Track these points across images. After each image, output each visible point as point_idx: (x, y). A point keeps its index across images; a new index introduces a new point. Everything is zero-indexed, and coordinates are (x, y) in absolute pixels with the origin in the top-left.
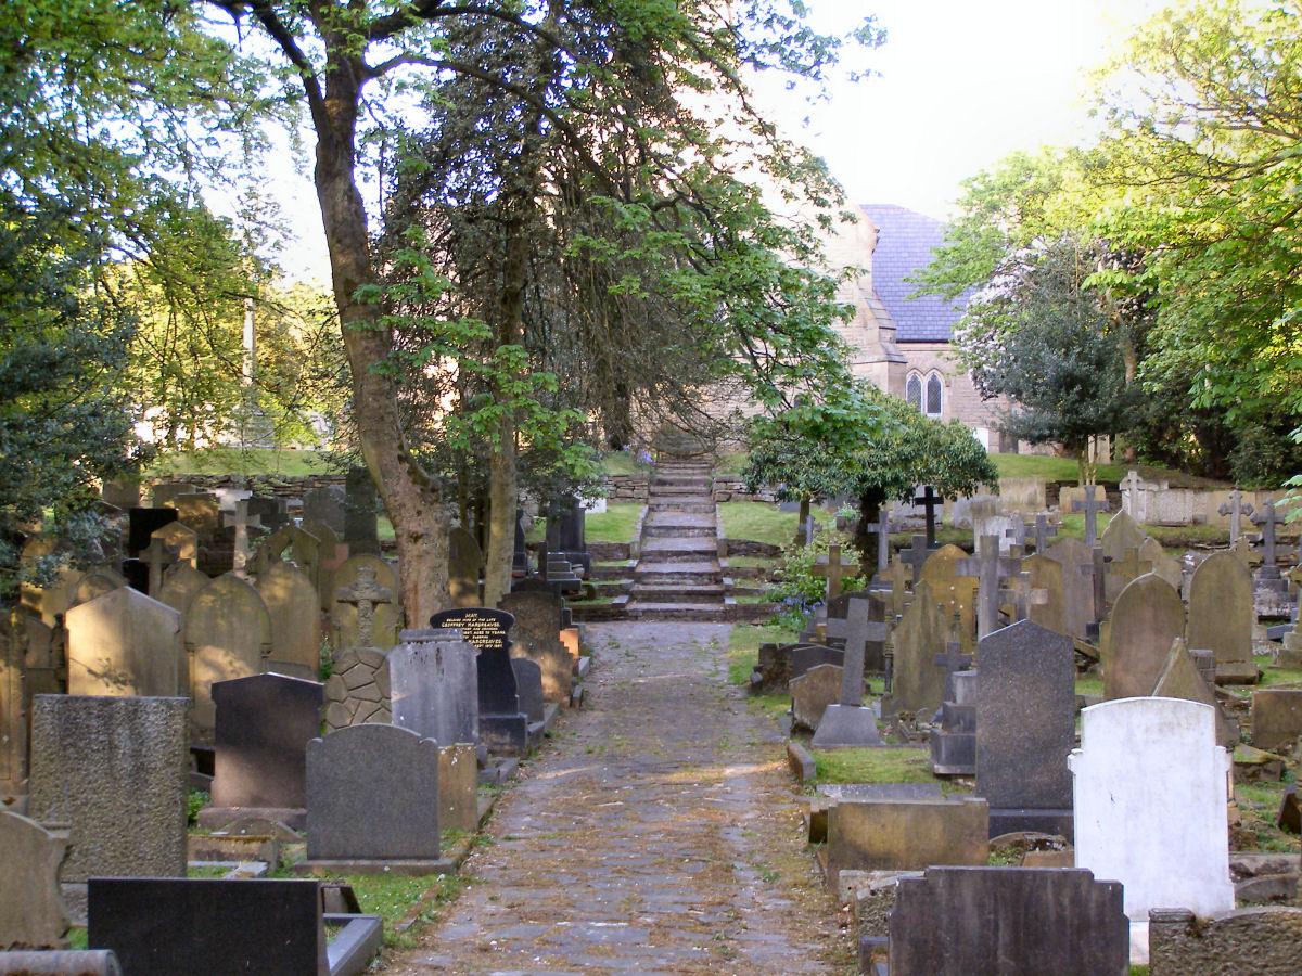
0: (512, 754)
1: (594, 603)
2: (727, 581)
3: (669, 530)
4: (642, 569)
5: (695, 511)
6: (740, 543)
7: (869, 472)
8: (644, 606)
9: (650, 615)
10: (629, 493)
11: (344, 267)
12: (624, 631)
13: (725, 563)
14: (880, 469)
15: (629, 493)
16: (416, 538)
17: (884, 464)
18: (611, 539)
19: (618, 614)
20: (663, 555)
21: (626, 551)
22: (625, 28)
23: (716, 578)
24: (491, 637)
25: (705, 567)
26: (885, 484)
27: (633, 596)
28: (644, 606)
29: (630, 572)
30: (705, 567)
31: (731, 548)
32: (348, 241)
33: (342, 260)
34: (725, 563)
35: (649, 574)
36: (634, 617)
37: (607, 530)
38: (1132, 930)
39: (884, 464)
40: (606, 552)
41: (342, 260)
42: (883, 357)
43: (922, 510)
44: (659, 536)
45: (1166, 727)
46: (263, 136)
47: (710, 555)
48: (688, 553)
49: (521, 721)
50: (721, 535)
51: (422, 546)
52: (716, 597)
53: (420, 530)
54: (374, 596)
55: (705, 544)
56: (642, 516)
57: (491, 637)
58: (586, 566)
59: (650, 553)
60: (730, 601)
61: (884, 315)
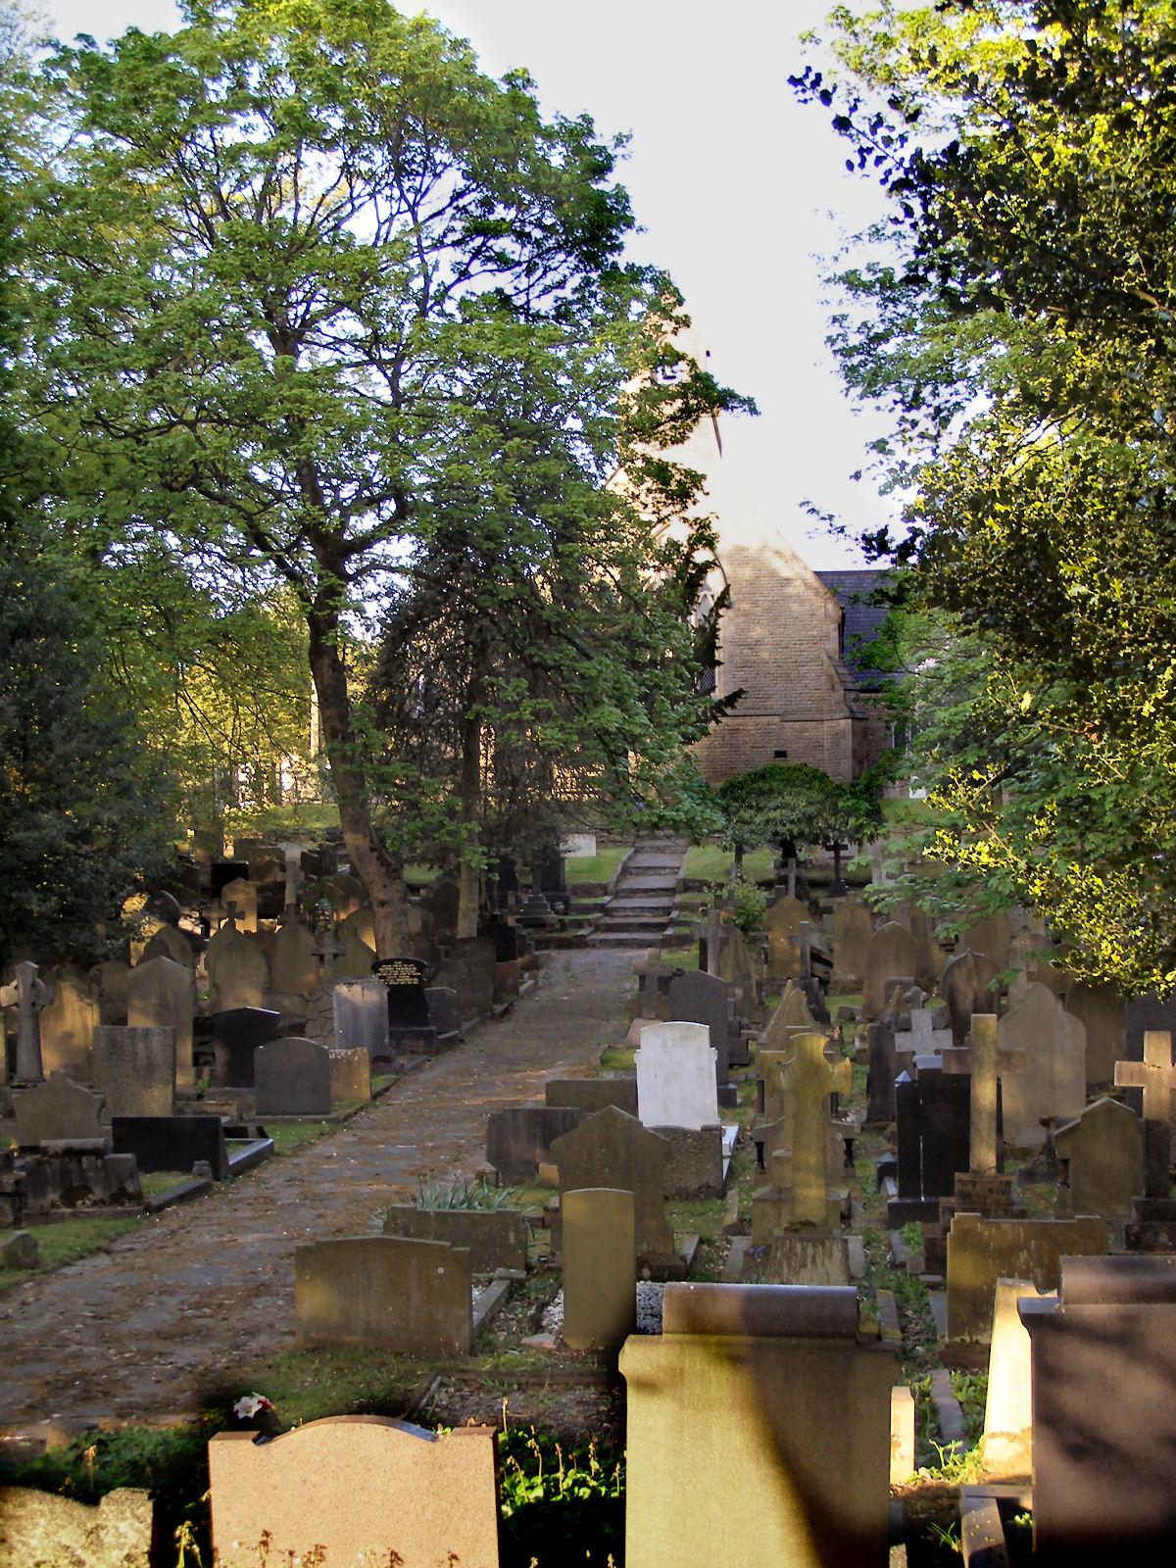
0: (425, 1053)
1: (564, 935)
2: (674, 914)
3: (645, 870)
4: (614, 904)
5: (673, 852)
6: (694, 881)
7: (780, 828)
8: (602, 936)
9: (604, 943)
10: (619, 838)
11: (330, 717)
12: (580, 958)
13: (678, 898)
14: (788, 826)
15: (619, 838)
16: (383, 904)
17: (792, 822)
18: (584, 880)
19: (580, 943)
20: (633, 893)
21: (604, 889)
22: (245, 754)
23: (667, 910)
24: (412, 976)
25: (665, 902)
26: (793, 837)
27: (597, 928)
28: (602, 936)
29: (601, 908)
30: (665, 902)
31: (687, 886)
32: (332, 699)
33: (328, 713)
34: (678, 898)
35: (616, 909)
36: (593, 945)
37: (591, 871)
38: (155, 1115)
39: (792, 822)
40: (588, 890)
41: (328, 713)
42: (848, 714)
43: (832, 854)
44: (638, 875)
45: (683, 1038)
46: (630, 267)
47: (670, 892)
48: (653, 890)
49: (430, 1033)
50: (682, 874)
51: (387, 909)
52: (662, 927)
53: (386, 898)
54: (335, 951)
55: (668, 882)
56: (625, 858)
57: (412, 976)
58: (566, 901)
59: (624, 890)
60: (669, 932)
61: (849, 679)
